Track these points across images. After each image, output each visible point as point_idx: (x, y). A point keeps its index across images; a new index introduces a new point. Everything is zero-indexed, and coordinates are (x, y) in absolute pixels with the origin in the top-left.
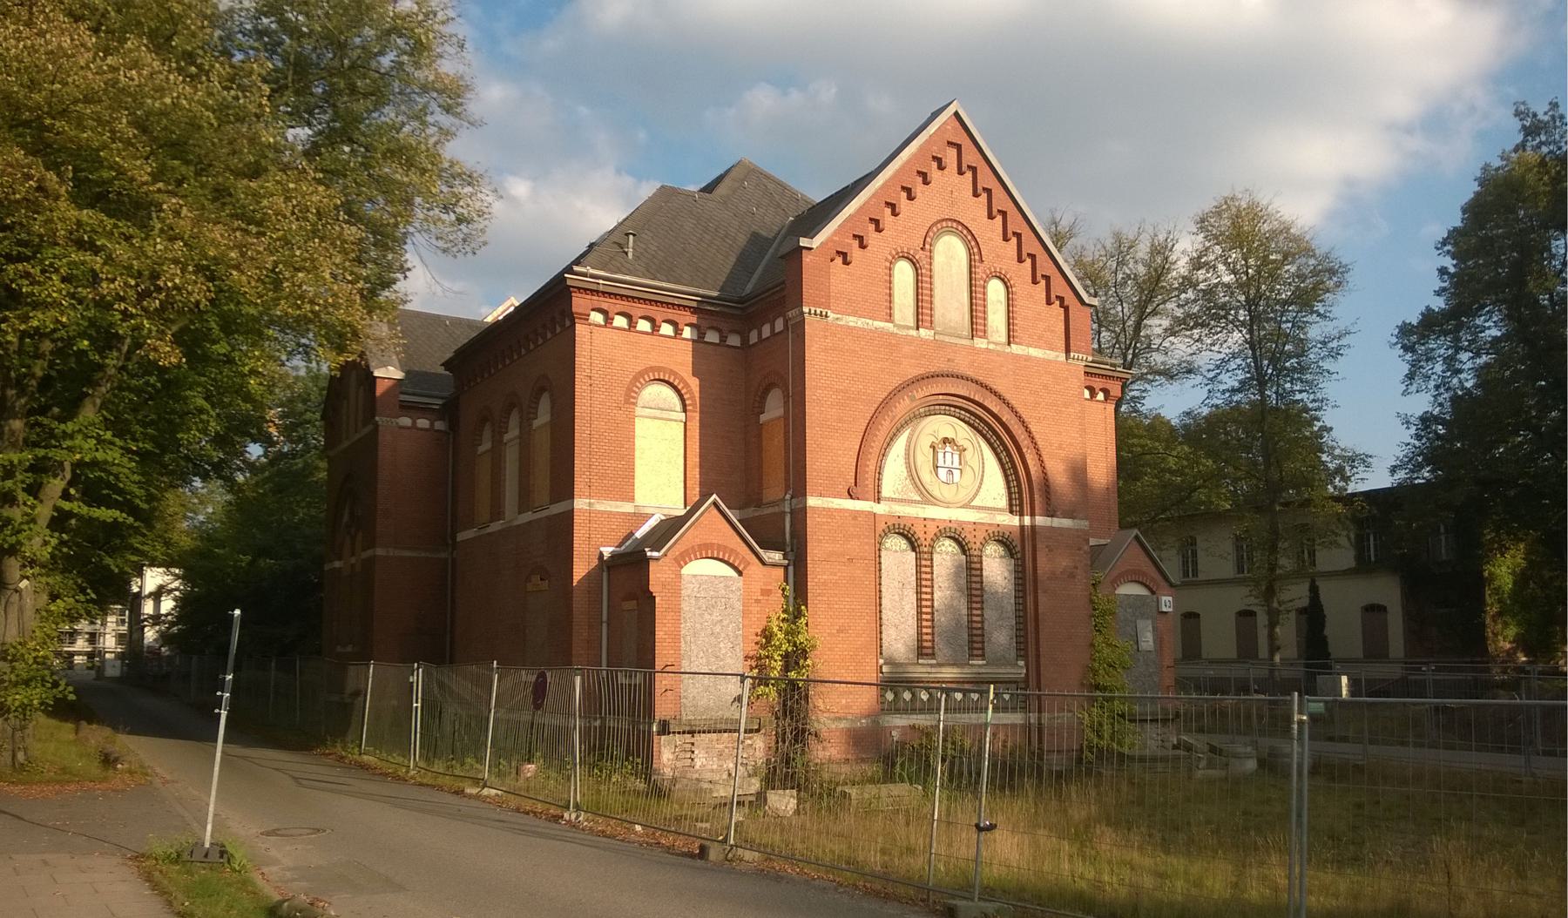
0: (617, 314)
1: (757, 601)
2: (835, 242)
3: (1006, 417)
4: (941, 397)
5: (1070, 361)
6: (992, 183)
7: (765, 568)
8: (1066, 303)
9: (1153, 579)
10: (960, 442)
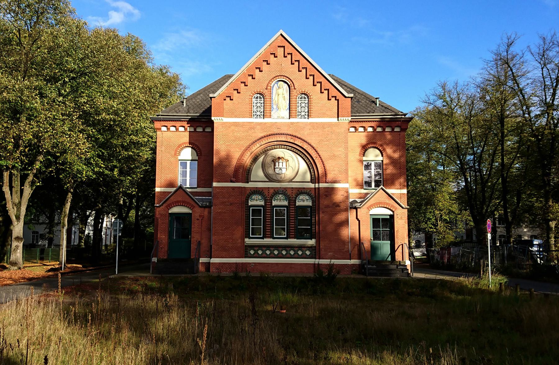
0: (171, 126)
1: (198, 219)
2: (226, 93)
3: (306, 146)
4: (276, 142)
5: (339, 121)
6: (299, 57)
7: (404, 209)
8: (337, 98)
9: (392, 206)
10: (286, 158)
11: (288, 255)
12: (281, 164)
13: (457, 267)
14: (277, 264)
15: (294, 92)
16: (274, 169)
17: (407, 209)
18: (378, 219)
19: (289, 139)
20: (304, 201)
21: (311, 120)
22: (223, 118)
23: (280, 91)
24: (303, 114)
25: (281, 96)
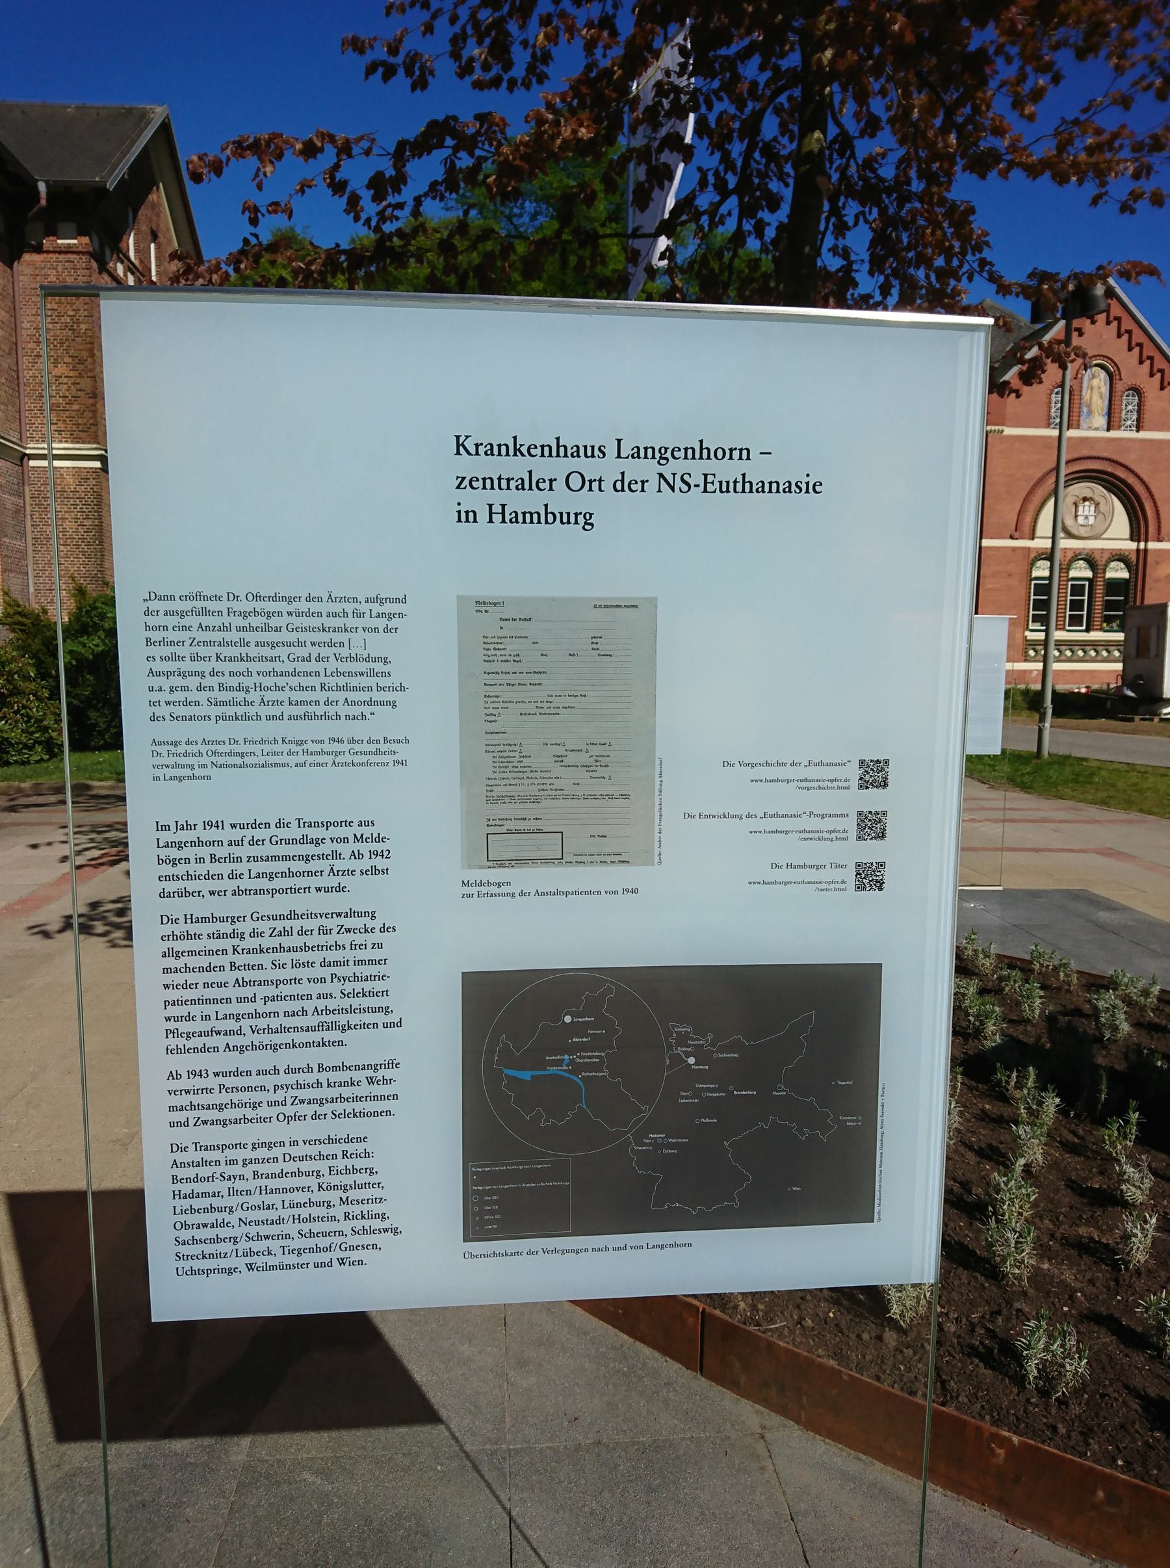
3: (1131, 480)
10: (1096, 498)
11: (1087, 658)
12: (1087, 508)
13: (934, 61)
14: (1073, 671)
15: (1119, 386)
16: (1076, 516)
17: (45, 249)
18: (496, 828)
19: (1109, 468)
20: (1117, 572)
21: (1143, 435)
22: (1005, 428)
23: (1095, 382)
24: (1129, 423)
25: (1095, 391)
